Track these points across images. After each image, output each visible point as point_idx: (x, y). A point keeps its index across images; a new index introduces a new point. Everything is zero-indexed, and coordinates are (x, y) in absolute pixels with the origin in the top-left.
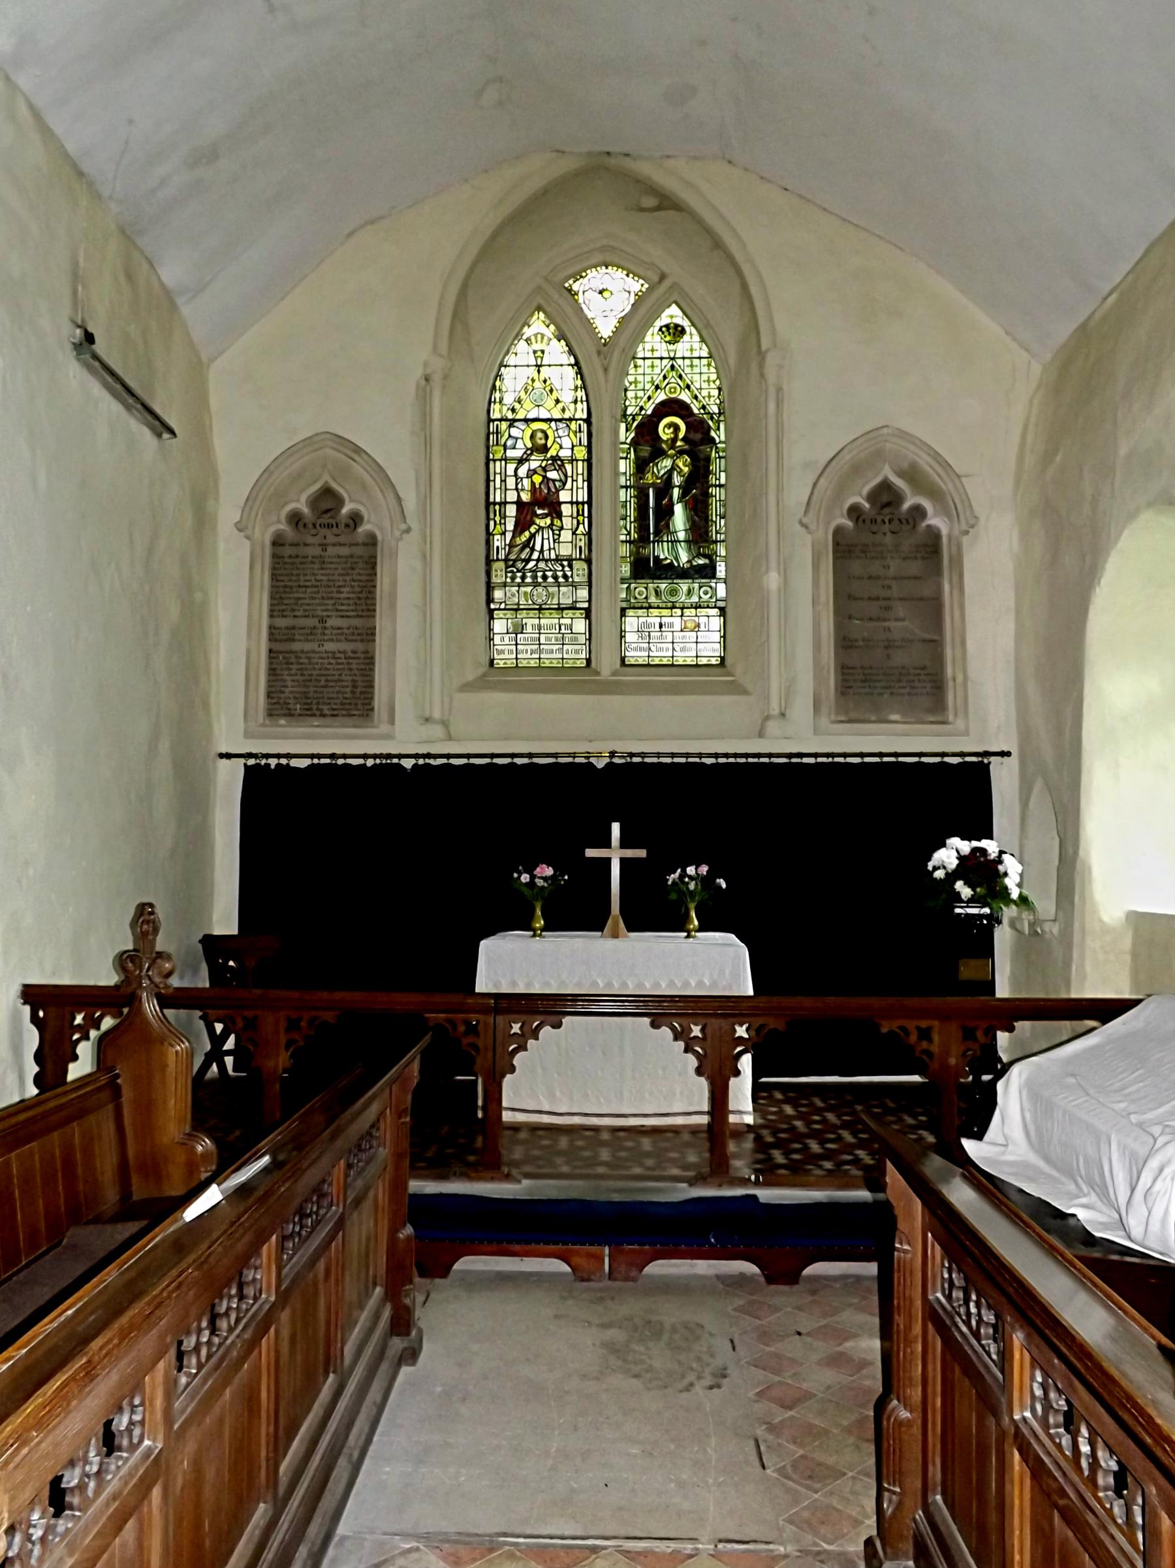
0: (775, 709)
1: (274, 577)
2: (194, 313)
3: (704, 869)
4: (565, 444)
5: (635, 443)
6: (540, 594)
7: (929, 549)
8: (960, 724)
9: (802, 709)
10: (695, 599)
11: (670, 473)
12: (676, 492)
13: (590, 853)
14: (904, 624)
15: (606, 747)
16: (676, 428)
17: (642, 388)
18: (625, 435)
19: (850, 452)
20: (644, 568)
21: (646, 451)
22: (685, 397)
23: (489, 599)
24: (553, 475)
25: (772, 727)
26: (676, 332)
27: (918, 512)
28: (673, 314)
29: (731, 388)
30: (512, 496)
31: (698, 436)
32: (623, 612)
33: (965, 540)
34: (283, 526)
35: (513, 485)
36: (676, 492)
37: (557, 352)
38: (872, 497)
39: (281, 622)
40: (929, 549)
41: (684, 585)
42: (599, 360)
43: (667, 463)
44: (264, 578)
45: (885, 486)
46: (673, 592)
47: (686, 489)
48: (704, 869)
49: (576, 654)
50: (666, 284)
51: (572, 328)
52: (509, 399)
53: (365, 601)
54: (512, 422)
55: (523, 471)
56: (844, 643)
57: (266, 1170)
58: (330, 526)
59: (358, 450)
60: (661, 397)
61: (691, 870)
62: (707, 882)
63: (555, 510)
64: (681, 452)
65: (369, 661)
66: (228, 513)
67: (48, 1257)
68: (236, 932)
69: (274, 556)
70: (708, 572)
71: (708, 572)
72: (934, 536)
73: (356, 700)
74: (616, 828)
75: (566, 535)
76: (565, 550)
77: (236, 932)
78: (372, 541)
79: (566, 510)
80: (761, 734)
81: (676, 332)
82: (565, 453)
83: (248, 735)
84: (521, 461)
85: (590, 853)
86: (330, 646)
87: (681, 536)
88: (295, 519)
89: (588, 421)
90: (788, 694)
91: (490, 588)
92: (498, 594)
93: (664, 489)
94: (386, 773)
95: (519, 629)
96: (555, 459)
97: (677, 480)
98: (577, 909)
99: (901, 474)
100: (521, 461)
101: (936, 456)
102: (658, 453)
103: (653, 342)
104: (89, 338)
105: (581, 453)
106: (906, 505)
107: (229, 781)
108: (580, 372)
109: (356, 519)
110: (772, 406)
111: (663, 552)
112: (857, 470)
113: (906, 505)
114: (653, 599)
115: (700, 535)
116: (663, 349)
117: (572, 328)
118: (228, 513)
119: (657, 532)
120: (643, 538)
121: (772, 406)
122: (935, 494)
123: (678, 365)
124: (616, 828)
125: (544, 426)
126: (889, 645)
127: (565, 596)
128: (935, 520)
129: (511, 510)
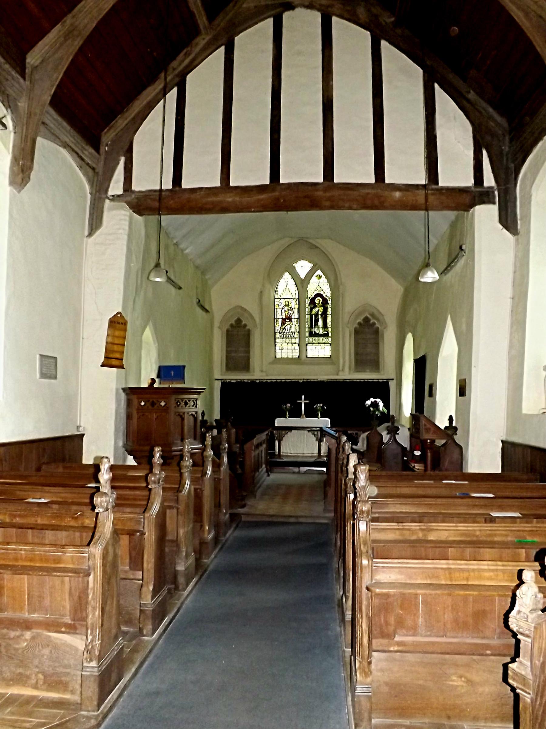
0: (341, 368)
2: (210, 282)
3: (321, 405)
4: (294, 304)
5: (310, 304)
6: (287, 341)
8: (382, 372)
9: (347, 369)
10: (324, 341)
11: (318, 311)
12: (319, 316)
13: (298, 401)
14: (370, 349)
15: (302, 377)
16: (320, 301)
17: (311, 291)
18: (308, 302)
19: (110, 617)
21: (312, 306)
22: (322, 293)
23: (275, 342)
24: (290, 312)
25: (341, 373)
26: (320, 277)
27: (374, 324)
28: (319, 272)
29: (334, 288)
30: (281, 317)
31: (325, 302)
32: (307, 345)
33: (385, 330)
35: (280, 315)
36: (319, 316)
37: (291, 282)
39: (229, 349)
41: (321, 338)
42: (301, 284)
43: (317, 309)
44: (225, 340)
46: (319, 340)
47: (322, 315)
48: (321, 405)
49: (296, 355)
50: (317, 266)
51: (295, 275)
52: (280, 294)
53: (248, 344)
54: (281, 299)
55: (283, 311)
56: (356, 354)
57: (488, 152)
58: (239, 327)
59: (246, 310)
60: (316, 293)
61: (319, 405)
62: (322, 407)
63: (291, 320)
64: (321, 306)
66: (217, 324)
68: (83, 463)
70: (327, 335)
71: (327, 335)
72: (378, 328)
73: (246, 367)
74: (303, 397)
75: (293, 326)
76: (293, 330)
77: (83, 463)
78: (249, 331)
79: (293, 320)
80: (337, 375)
81: (320, 277)
82: (293, 307)
83: (221, 375)
84: (283, 308)
85: (298, 401)
86: (240, 355)
87: (321, 326)
89: (299, 299)
91: (275, 339)
92: (277, 340)
93: (317, 315)
94: (253, 383)
95: (282, 349)
96: (290, 308)
97: (320, 313)
98: (295, 413)
99: (370, 315)
100: (283, 308)
101: (378, 311)
102: (315, 306)
103: (314, 279)
104: (199, 301)
105: (297, 306)
106: (371, 322)
107: (218, 386)
108: (297, 286)
109: (245, 326)
110: (341, 298)
111: (316, 330)
112: (360, 314)
113: (371, 322)
114: (314, 341)
115: (325, 326)
116: (317, 281)
117: (295, 275)
118: (217, 324)
119: (315, 325)
120: (312, 327)
121: (341, 298)
122: (378, 320)
123: (320, 285)
124: (303, 397)
125: (288, 300)
127: (293, 341)
128: (377, 325)
129: (280, 320)
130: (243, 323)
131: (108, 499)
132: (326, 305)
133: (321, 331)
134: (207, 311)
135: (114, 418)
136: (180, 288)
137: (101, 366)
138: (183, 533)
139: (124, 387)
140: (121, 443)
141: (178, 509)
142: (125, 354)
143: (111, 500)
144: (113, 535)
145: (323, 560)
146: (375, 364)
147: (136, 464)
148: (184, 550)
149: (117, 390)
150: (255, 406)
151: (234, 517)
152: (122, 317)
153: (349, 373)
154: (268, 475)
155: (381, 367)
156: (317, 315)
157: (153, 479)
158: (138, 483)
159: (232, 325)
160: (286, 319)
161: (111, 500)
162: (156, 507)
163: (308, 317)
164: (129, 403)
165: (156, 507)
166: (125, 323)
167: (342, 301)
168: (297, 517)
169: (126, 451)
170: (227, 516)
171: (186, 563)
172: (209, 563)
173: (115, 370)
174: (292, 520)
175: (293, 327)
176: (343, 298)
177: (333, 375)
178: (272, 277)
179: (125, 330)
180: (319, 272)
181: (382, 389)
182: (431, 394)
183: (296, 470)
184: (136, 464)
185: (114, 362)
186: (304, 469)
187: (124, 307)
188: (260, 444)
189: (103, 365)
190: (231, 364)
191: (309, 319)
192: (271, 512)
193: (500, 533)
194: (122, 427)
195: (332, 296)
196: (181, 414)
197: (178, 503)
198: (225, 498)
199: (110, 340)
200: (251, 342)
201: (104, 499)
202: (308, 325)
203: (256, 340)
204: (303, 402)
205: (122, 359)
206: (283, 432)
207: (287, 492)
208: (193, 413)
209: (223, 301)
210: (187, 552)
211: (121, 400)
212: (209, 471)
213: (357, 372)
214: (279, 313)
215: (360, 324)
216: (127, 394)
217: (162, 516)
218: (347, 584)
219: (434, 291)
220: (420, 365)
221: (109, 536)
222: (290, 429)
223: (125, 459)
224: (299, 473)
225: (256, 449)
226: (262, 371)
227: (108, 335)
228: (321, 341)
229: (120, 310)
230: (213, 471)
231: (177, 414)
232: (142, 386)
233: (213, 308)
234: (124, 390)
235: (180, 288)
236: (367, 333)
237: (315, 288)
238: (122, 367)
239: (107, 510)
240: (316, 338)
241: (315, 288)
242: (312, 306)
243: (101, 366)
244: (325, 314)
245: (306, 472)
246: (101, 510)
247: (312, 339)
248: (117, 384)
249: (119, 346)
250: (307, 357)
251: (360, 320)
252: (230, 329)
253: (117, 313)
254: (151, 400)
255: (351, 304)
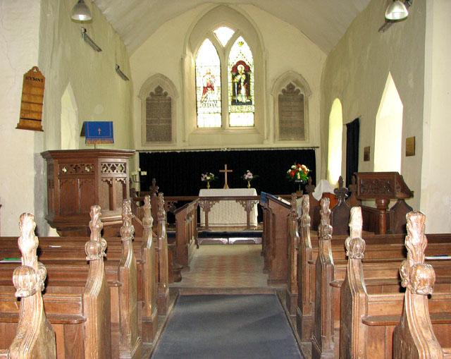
1: (147, 108)
4: (217, 72)
7: (204, 269)
10: (247, 110)
12: (242, 84)
17: (233, 59)
18: (230, 69)
20: (235, 102)
21: (234, 74)
22: (244, 60)
25: (266, 142)
26: (242, 43)
27: (299, 91)
34: (149, 96)
35: (201, 83)
38: (288, 87)
40: (204, 269)
42: (223, 52)
44: (145, 108)
45: (291, 84)
56: (281, 122)
63: (212, 88)
65: (170, 128)
66: (136, 92)
67: (369, 309)
69: (147, 103)
70: (250, 103)
72: (303, 95)
73: (168, 137)
78: (170, 99)
80: (262, 143)
81: (242, 43)
82: (215, 75)
88: (152, 94)
90: (268, 134)
93: (239, 83)
94: (173, 156)
97: (242, 81)
98: (217, 184)
102: (238, 74)
109: (166, 94)
110: (264, 66)
111: (239, 98)
112: (284, 80)
114: (237, 110)
115: (248, 94)
117: (216, 43)
118: (136, 92)
120: (234, 95)
122: (302, 87)
123: (242, 52)
126: (291, 122)
129: (202, 89)
130: (163, 92)
131: (34, 275)
132: (249, 73)
133: (244, 100)
134: (125, 78)
135: (33, 186)
136: (100, 50)
137: (17, 128)
138: (128, 315)
139: (43, 151)
140: (42, 215)
141: (119, 286)
142: (43, 115)
143: (39, 279)
144: (45, 328)
145: (84, 280)
146: (301, 132)
147: (58, 236)
148: (129, 335)
149: (36, 155)
150: (177, 176)
151: (174, 291)
152: (39, 73)
153: (274, 142)
154: (198, 248)
155: (306, 135)
156: (239, 83)
157: (92, 248)
158: (66, 256)
159: (152, 94)
160: (208, 87)
161: (39, 279)
162: (97, 284)
163: (230, 85)
164: (50, 169)
165: (97, 284)
166: (42, 80)
167: (266, 67)
168: (239, 289)
169: (49, 222)
170: (168, 291)
171: (126, 345)
172: (154, 345)
173: (32, 132)
174: (234, 293)
175: (215, 95)
177: (256, 144)
178: (193, 43)
179: (43, 88)
180: (241, 39)
181: (307, 157)
182: (367, 158)
183: (225, 240)
184: (58, 236)
185: (29, 123)
186: (232, 240)
187: (41, 60)
188: (189, 215)
189: (19, 127)
190: (152, 135)
191: (231, 87)
192: (211, 286)
193: (436, 298)
194: (44, 196)
195: (255, 64)
196: (109, 180)
197: (119, 280)
198: (165, 272)
199: (26, 99)
200: (173, 110)
201: (28, 277)
202: (230, 93)
203: (177, 109)
204: (226, 171)
205: (41, 120)
206: (211, 203)
207: (222, 265)
208: (122, 179)
209: (143, 67)
210: (132, 337)
211: (40, 166)
212: (150, 241)
213: (282, 140)
215: (284, 91)
216: (47, 159)
217: (105, 295)
219: (368, 51)
220: (353, 131)
221: (38, 331)
222: (217, 199)
223: (47, 231)
224: (228, 243)
225: (186, 218)
226: (184, 141)
227: (23, 93)
228: (244, 110)
229: (37, 65)
230: (154, 241)
231: (104, 180)
232: (62, 149)
233: (132, 76)
234: (43, 154)
235: (100, 50)
236: (291, 100)
238: (40, 129)
239: (34, 293)
240: (239, 107)
243: (17, 128)
244: (247, 81)
245: (236, 243)
246: (25, 294)
247: (235, 108)
248: (35, 149)
249: (37, 105)
251: (284, 87)
252: (151, 98)
253: (34, 68)
254: (75, 165)
255: (275, 70)
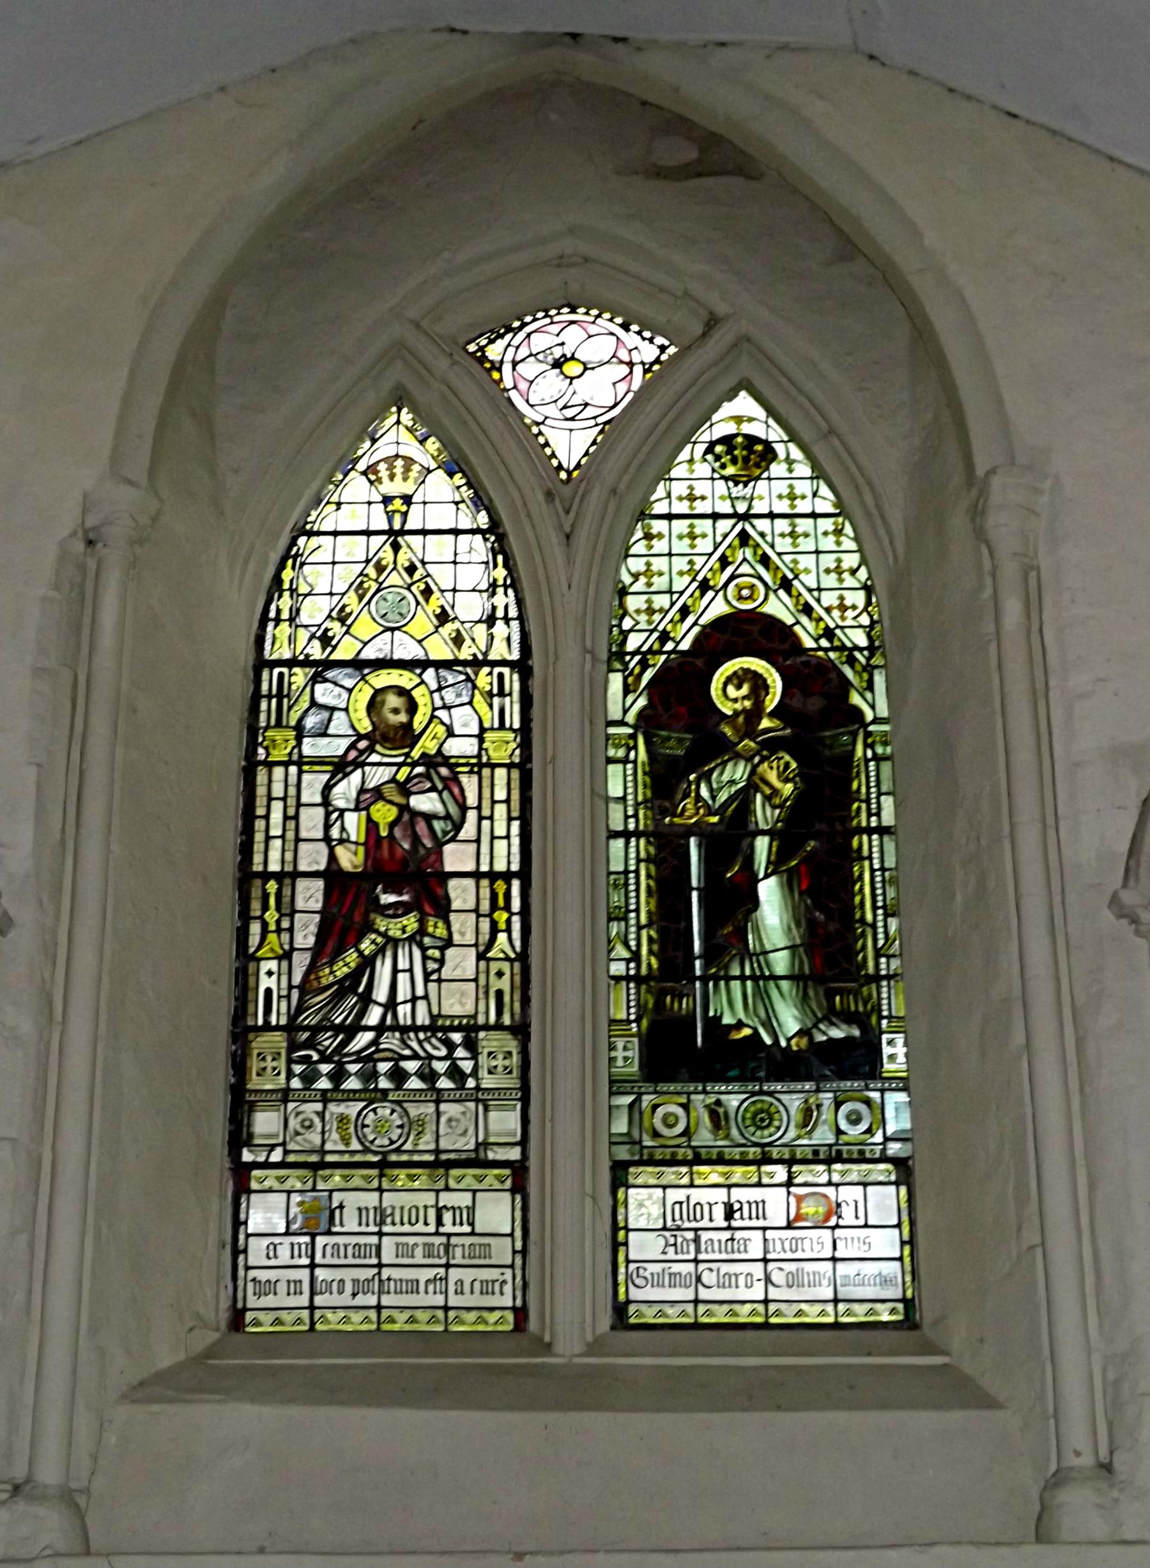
10: (823, 1136)
11: (744, 798)
16: (759, 685)
17: (669, 576)
18: (620, 701)
21: (676, 747)
22: (779, 608)
26: (749, 457)
35: (317, 825)
42: (553, 522)
46: (763, 1118)
47: (786, 840)
55: (346, 790)
63: (428, 891)
64: (771, 746)
71: (857, 1061)
75: (461, 962)
76: (457, 1002)
79: (461, 894)
84: (340, 767)
91: (241, 1105)
92: (265, 1122)
93: (729, 836)
97: (763, 814)
100: (340, 767)
111: (731, 1006)
115: (831, 955)
116: (716, 495)
117: (486, 448)
121: (1013, 608)
123: (762, 532)
125: (405, 679)
129: (310, 896)
176: (1033, 604)
180: (743, 413)
214: (292, 818)
218: (57, 969)
237: (705, 567)
241: (705, 567)
242: (676, 747)
250: (620, 1310)
